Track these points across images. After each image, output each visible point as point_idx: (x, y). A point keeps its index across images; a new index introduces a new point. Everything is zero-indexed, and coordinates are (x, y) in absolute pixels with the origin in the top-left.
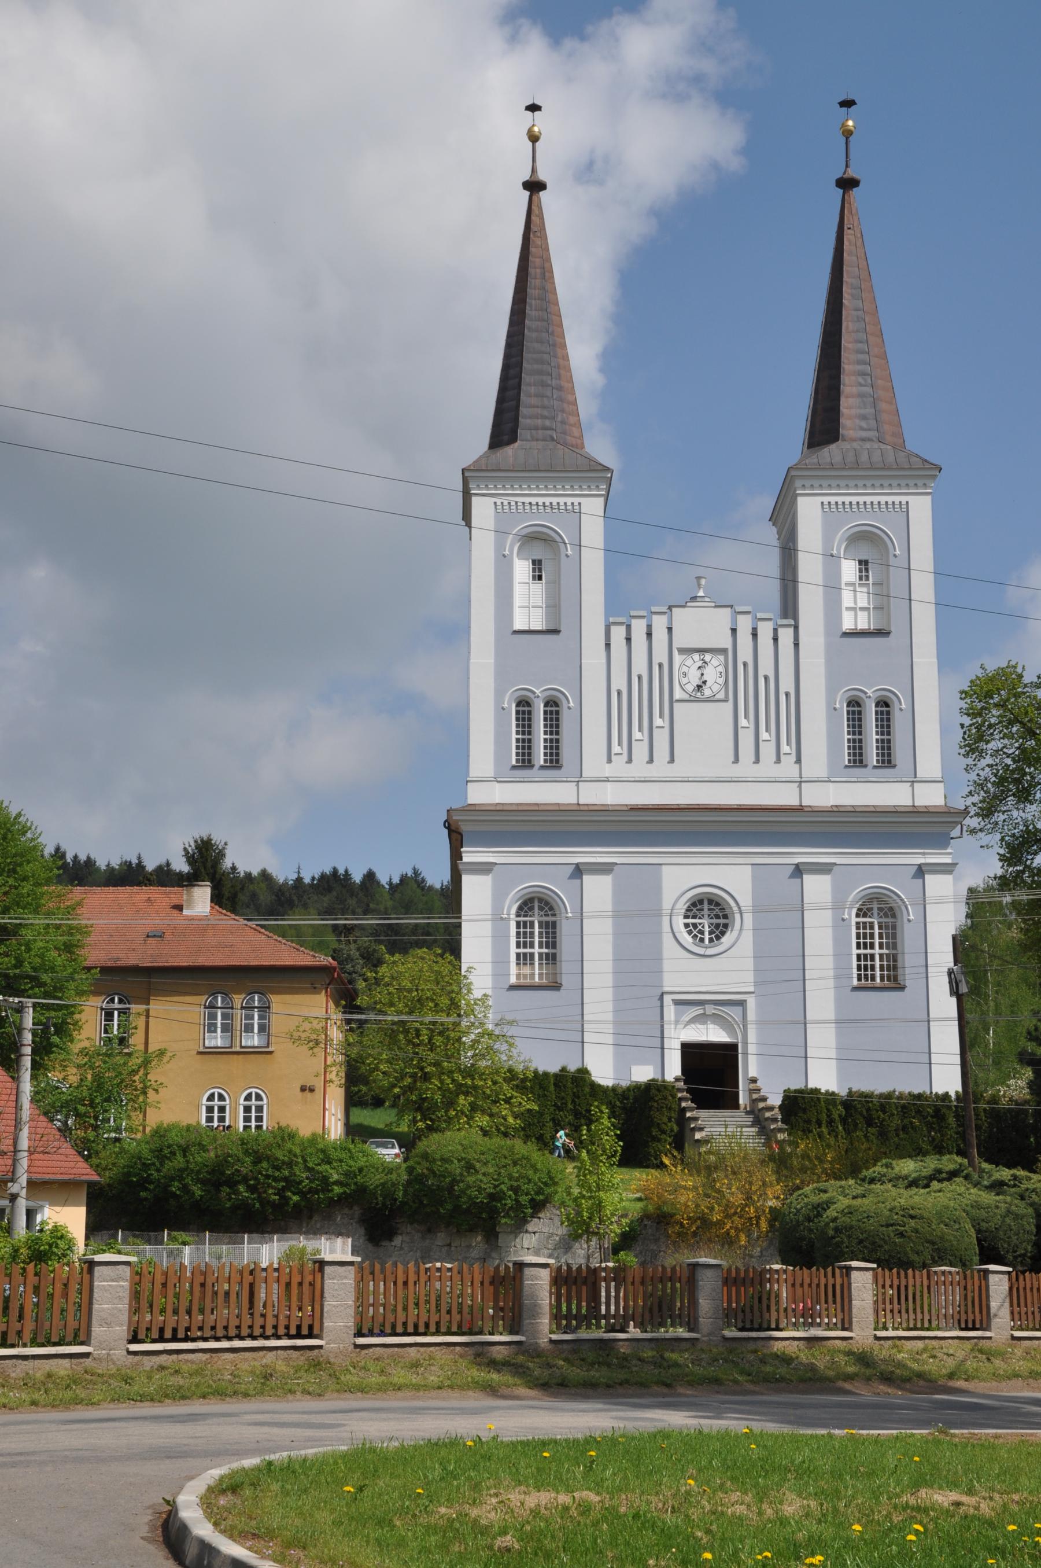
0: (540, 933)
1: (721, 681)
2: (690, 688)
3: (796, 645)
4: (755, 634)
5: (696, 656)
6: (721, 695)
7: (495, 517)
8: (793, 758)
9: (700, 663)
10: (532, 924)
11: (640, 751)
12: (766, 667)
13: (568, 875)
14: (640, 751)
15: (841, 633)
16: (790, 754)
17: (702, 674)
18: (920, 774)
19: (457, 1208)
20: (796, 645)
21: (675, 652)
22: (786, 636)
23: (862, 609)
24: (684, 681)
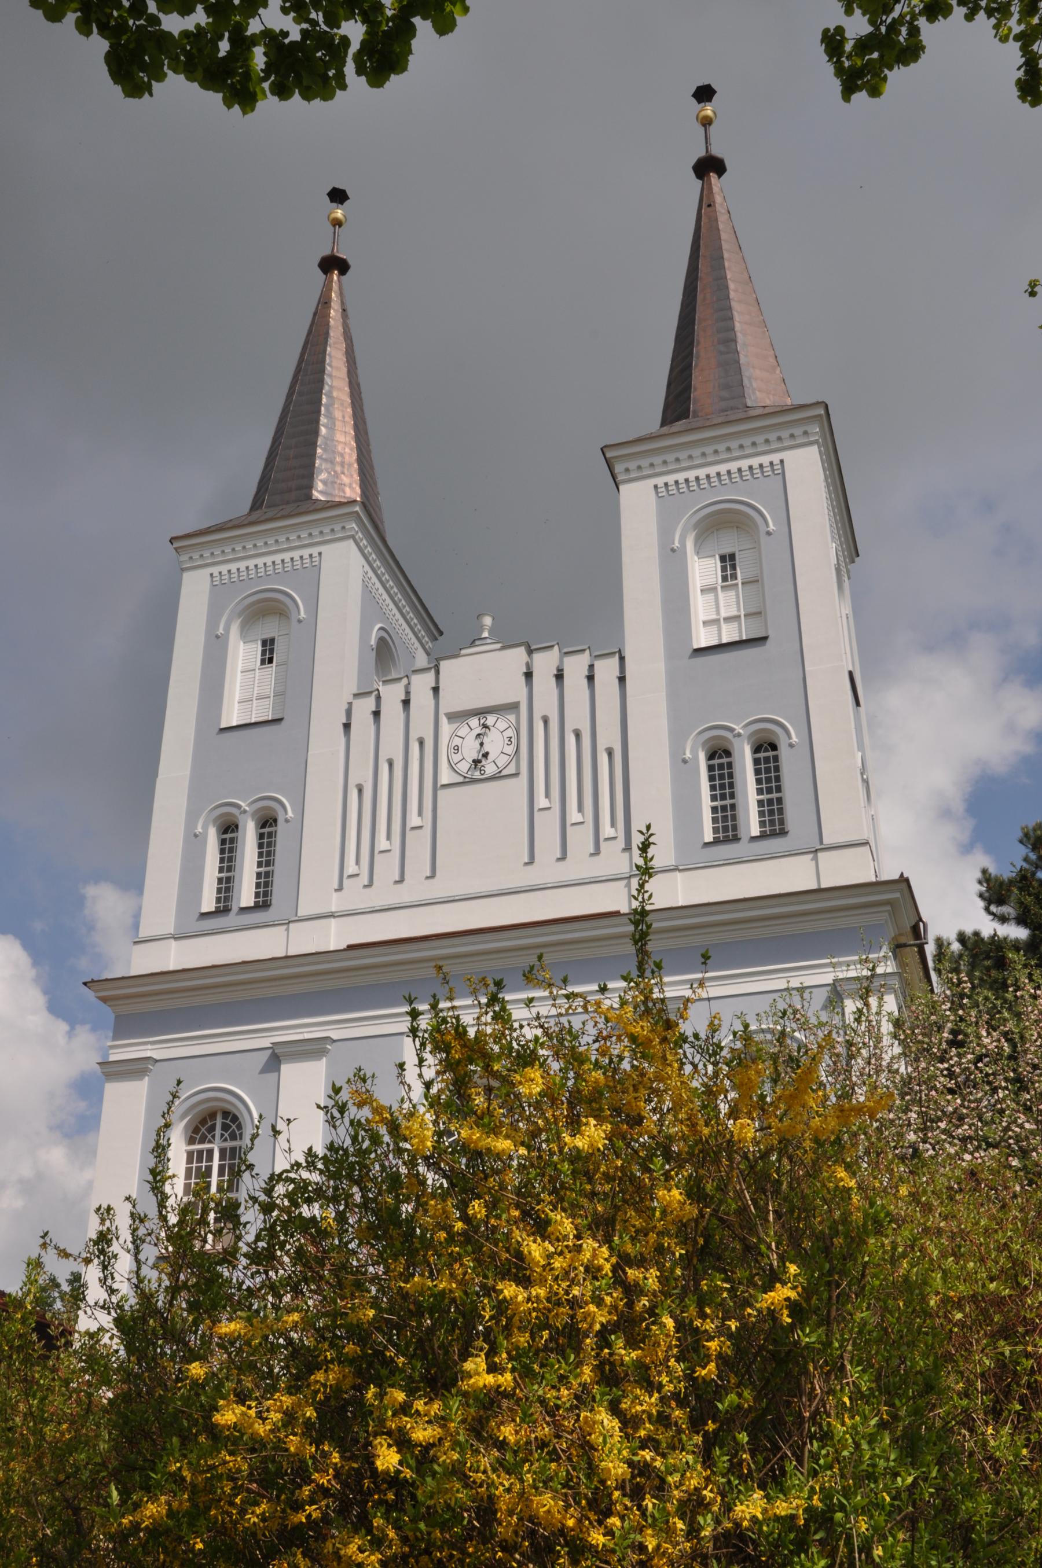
0: (221, 1169)
1: (510, 750)
2: (464, 767)
3: (622, 679)
4: (559, 677)
5: (474, 722)
6: (511, 769)
7: (211, 592)
8: (621, 843)
9: (479, 730)
10: (210, 1152)
11: (387, 868)
12: (577, 717)
13: (260, 1067)
14: (387, 868)
15: (691, 651)
16: (615, 838)
17: (482, 744)
18: (827, 840)
19: (995, 1375)
20: (622, 679)
21: (444, 720)
22: (607, 670)
23: (727, 619)
24: (456, 758)
